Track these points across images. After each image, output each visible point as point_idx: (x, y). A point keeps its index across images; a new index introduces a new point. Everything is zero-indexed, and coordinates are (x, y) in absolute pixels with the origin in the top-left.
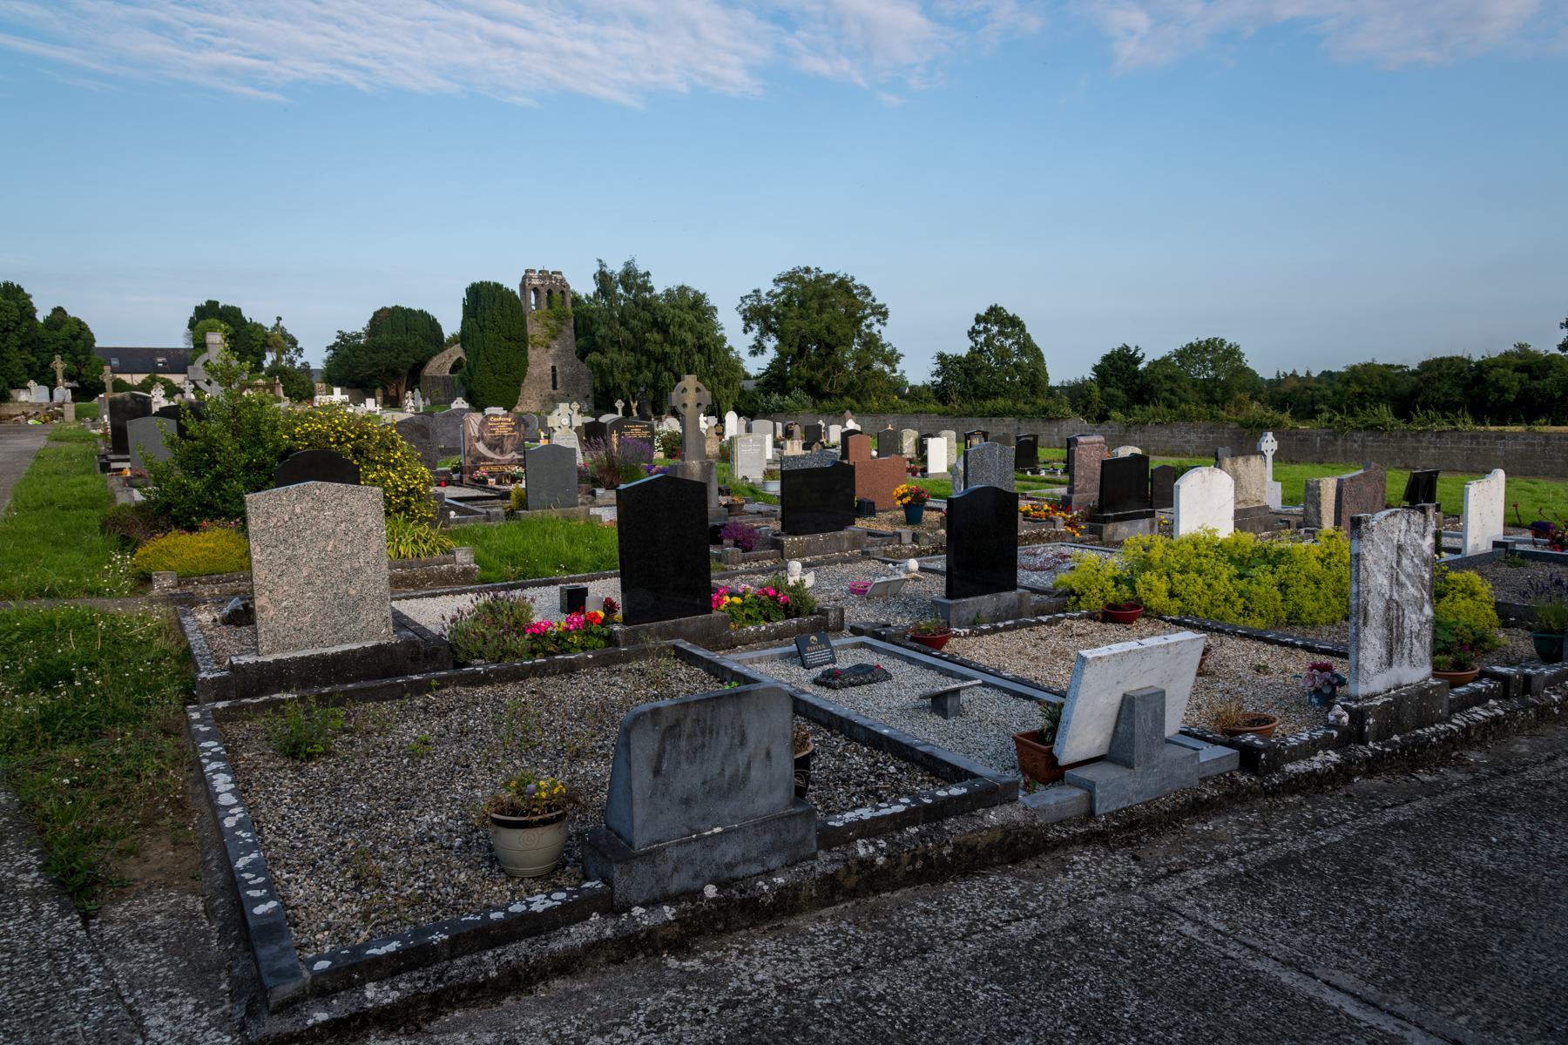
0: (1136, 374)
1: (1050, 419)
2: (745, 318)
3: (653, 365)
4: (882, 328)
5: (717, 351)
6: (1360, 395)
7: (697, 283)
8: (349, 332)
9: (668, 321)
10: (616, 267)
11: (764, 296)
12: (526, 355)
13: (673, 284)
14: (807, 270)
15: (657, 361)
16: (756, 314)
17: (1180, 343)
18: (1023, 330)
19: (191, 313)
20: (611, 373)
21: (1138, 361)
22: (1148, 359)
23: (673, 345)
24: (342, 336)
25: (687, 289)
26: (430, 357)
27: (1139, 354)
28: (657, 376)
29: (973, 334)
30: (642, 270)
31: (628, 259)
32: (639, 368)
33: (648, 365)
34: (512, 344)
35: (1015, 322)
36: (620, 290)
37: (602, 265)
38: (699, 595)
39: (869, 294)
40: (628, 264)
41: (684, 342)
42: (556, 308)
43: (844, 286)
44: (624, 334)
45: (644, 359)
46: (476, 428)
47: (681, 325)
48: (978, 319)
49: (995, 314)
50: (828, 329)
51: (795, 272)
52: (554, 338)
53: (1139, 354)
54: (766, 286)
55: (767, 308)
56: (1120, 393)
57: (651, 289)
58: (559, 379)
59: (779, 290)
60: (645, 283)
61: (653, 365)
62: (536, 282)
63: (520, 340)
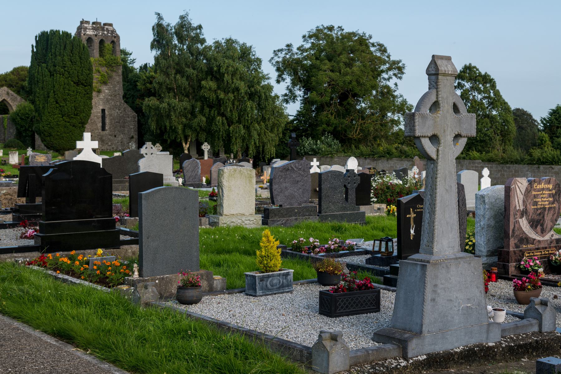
2: (278, 70)
3: (207, 110)
5: (267, 99)
9: (223, 70)
10: (172, 20)
11: (295, 50)
12: (91, 98)
13: (222, 37)
14: (331, 28)
15: (211, 107)
18: (493, 86)
20: (169, 116)
23: (226, 92)
25: (236, 42)
30: (195, 24)
31: (183, 13)
34: (80, 89)
35: (486, 79)
36: (175, 41)
37: (160, 17)
39: (385, 51)
40: (182, 18)
41: (237, 89)
42: (108, 56)
43: (362, 43)
44: (183, 81)
46: (521, 197)
47: (234, 74)
50: (358, 82)
51: (319, 30)
52: (105, 83)
54: (297, 42)
55: (298, 62)
57: (203, 41)
58: (107, 121)
59: (308, 46)
60: (197, 35)
62: (90, 32)
63: (85, 85)
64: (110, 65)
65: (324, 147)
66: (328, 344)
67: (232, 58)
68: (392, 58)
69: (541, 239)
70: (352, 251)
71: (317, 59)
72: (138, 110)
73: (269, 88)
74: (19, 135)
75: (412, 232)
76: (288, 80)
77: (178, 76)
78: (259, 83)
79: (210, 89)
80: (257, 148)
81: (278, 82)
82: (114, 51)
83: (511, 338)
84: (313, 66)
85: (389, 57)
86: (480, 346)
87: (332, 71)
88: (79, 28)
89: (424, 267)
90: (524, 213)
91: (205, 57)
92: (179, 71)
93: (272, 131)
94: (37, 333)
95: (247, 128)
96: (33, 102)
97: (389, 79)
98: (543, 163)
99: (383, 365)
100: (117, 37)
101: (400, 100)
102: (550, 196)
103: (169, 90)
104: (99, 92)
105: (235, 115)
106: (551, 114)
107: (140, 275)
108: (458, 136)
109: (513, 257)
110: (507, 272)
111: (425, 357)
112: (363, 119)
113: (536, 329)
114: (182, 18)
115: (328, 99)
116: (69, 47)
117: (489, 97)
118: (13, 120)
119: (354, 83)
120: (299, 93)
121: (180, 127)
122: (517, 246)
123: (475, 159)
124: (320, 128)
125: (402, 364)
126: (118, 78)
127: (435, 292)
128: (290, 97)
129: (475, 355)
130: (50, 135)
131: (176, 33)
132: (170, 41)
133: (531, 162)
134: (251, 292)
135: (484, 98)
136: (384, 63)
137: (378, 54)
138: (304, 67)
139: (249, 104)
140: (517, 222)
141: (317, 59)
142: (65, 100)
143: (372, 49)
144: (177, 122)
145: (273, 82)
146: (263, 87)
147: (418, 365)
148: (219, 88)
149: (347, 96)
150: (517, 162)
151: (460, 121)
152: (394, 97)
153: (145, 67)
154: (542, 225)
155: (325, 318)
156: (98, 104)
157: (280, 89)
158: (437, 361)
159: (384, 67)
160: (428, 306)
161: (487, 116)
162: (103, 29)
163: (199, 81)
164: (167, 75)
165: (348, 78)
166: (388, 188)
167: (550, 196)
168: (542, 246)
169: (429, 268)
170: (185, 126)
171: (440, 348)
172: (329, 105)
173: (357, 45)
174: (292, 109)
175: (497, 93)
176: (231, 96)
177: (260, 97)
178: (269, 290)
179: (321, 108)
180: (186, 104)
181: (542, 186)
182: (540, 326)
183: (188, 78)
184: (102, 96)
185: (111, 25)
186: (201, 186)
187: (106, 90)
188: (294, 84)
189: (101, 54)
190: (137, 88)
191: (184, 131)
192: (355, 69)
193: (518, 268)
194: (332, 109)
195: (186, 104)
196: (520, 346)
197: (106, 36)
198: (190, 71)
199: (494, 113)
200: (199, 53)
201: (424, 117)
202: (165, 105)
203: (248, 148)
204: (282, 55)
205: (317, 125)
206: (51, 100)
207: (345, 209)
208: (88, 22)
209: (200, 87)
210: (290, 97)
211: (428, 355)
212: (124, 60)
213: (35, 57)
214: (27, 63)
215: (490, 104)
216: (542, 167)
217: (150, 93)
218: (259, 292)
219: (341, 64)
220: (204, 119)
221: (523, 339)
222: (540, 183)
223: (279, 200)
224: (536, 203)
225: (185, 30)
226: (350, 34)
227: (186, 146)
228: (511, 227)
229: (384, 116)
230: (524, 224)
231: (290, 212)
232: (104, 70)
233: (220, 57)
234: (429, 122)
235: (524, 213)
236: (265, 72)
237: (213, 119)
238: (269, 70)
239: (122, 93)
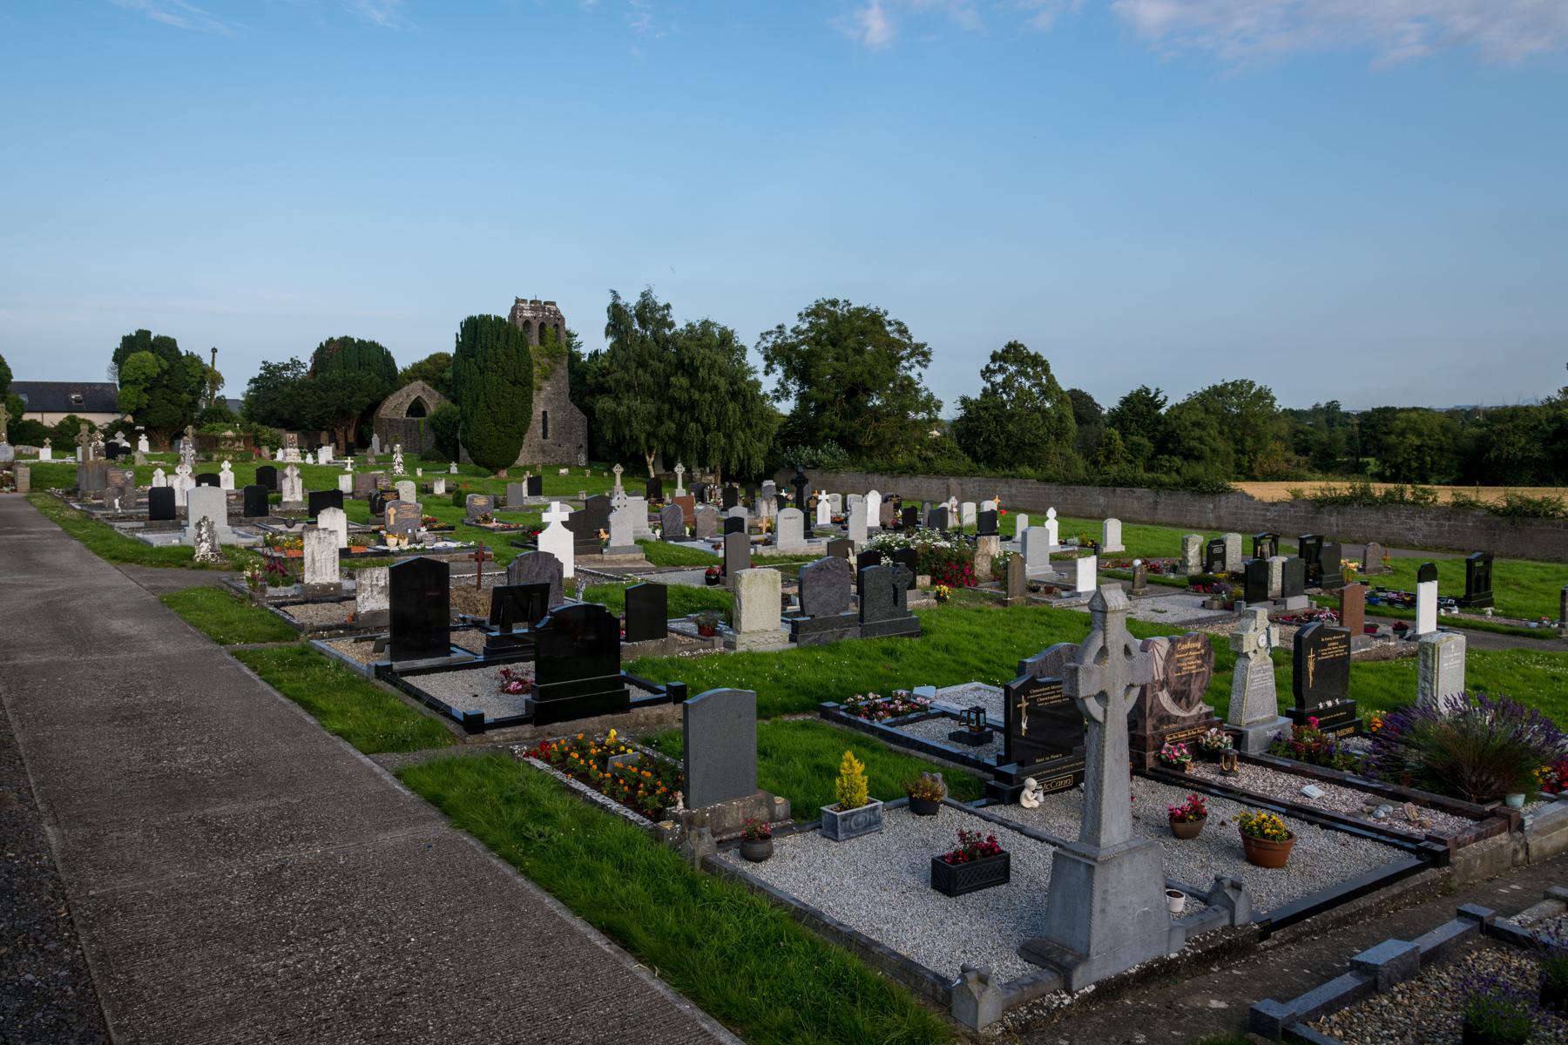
0: (1159, 419)
1: (1202, 493)
2: (767, 358)
3: (677, 414)
4: (922, 370)
5: (753, 399)
6: (1419, 448)
7: (723, 318)
8: (275, 363)
9: (697, 363)
11: (788, 332)
12: (531, 401)
13: (696, 319)
14: (834, 303)
15: (682, 409)
16: (777, 354)
17: (1201, 385)
18: (1046, 369)
19: (118, 344)
20: (628, 423)
21: (1159, 406)
22: (1169, 404)
23: (702, 390)
24: (267, 367)
26: (385, 396)
27: (1161, 397)
28: (682, 427)
29: (987, 373)
32: (659, 419)
33: (671, 413)
34: (518, 389)
35: (1037, 361)
38: (265, 513)
39: (905, 331)
41: (716, 387)
42: (550, 344)
44: (647, 378)
45: (666, 407)
46: (1161, 663)
47: (711, 367)
48: (994, 358)
49: (1013, 353)
52: (546, 378)
53: (1161, 397)
54: (791, 322)
55: (793, 347)
56: (1145, 441)
57: (671, 325)
58: (550, 426)
59: (805, 326)
60: (664, 317)
61: (677, 414)
62: (527, 314)
63: (524, 385)
64: (552, 355)
65: (826, 458)
66: (974, 987)
67: (709, 347)
68: (914, 340)
69: (1183, 714)
70: (925, 713)
71: (817, 344)
72: (589, 412)
73: (757, 385)
74: (439, 443)
75: (1024, 725)
76: (779, 371)
77: (640, 372)
78: (743, 378)
79: (681, 388)
80: (741, 462)
81: (767, 373)
82: (557, 338)
83: (1197, 940)
84: (810, 353)
85: (910, 338)
86: (1160, 960)
87: (837, 359)
88: (514, 309)
89: (1090, 868)
90: (1164, 684)
91: (674, 345)
92: (642, 364)
93: (760, 440)
94: (578, 924)
95: (728, 436)
96: (454, 401)
97: (910, 368)
98: (1121, 485)
99: (1041, 1006)
100: (562, 319)
101: (924, 394)
102: (1197, 657)
103: (629, 387)
104: (540, 389)
105: (713, 422)
106: (1122, 403)
107: (686, 806)
108: (1131, 686)
109: (1150, 742)
110: (1143, 764)
111: (1093, 987)
112: (877, 420)
113: (1226, 922)
114: (643, 295)
115: (832, 396)
116: (503, 337)
117: (1040, 385)
118: (432, 425)
119: (866, 376)
120: (793, 387)
121: (643, 436)
122: (1155, 728)
123: (1027, 477)
124: (821, 434)
125: (1066, 1002)
126: (563, 371)
127: (1104, 899)
128: (781, 393)
129: (1157, 973)
130: (480, 448)
131: (637, 315)
132: (629, 326)
133: (1103, 484)
134: (829, 833)
135: (1034, 385)
136: (905, 346)
137: (896, 336)
138: (799, 353)
139: (731, 406)
140: (1156, 697)
141: (817, 344)
142: (499, 404)
143: (888, 328)
144: (639, 430)
145: (761, 377)
146: (749, 384)
147: (1086, 999)
148: (692, 385)
149: (855, 391)
150: (1084, 483)
151: (1133, 668)
152: (918, 391)
153: (595, 355)
154: (1188, 697)
155: (940, 896)
156: (539, 406)
157: (769, 384)
158: (1109, 990)
159: (904, 353)
160: (1096, 921)
161: (1038, 409)
162: (544, 309)
163: (667, 377)
164: (627, 369)
165: (859, 369)
166: (932, 552)
167: (1197, 657)
168: (1188, 723)
169: (1098, 871)
170: (649, 435)
171: (1110, 972)
172: (832, 403)
173: (870, 323)
174: (786, 407)
175: (1051, 379)
176: (708, 396)
177: (745, 397)
178: (852, 831)
179: (821, 408)
180: (650, 407)
181: (1189, 645)
182: (1232, 917)
183: (653, 373)
184: (542, 395)
185: (553, 304)
186: (683, 539)
187: (547, 387)
188: (787, 377)
189: (542, 342)
190: (587, 382)
191: (647, 441)
192: (866, 356)
193: (1158, 758)
194: (837, 409)
195: (650, 407)
196: (1209, 952)
197: (548, 318)
198: (655, 364)
199: (1048, 405)
200: (667, 340)
201: (1088, 671)
202: (623, 409)
203: (729, 463)
204: (771, 339)
205: (818, 430)
206: (482, 404)
207: (893, 615)
208: (524, 301)
209: (668, 385)
210: (781, 393)
211: (1096, 984)
212: (569, 345)
213: (460, 346)
214: (451, 350)
215: (1043, 393)
216: (1118, 490)
217: (602, 390)
218: (841, 836)
219: (849, 351)
220: (673, 426)
221: (1211, 941)
222: (1184, 642)
223: (811, 608)
224: (1180, 669)
225: (649, 312)
226: (859, 309)
227: (650, 460)
228: (1148, 704)
229: (905, 417)
230: (1164, 698)
231: (826, 624)
232: (545, 361)
233: (692, 345)
234: (1096, 677)
235: (1164, 684)
236: (751, 365)
237: (686, 425)
238: (755, 360)
239: (567, 390)
